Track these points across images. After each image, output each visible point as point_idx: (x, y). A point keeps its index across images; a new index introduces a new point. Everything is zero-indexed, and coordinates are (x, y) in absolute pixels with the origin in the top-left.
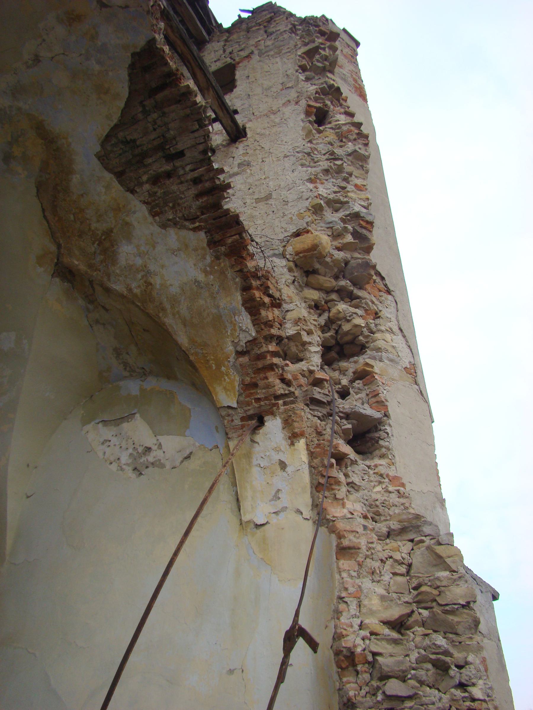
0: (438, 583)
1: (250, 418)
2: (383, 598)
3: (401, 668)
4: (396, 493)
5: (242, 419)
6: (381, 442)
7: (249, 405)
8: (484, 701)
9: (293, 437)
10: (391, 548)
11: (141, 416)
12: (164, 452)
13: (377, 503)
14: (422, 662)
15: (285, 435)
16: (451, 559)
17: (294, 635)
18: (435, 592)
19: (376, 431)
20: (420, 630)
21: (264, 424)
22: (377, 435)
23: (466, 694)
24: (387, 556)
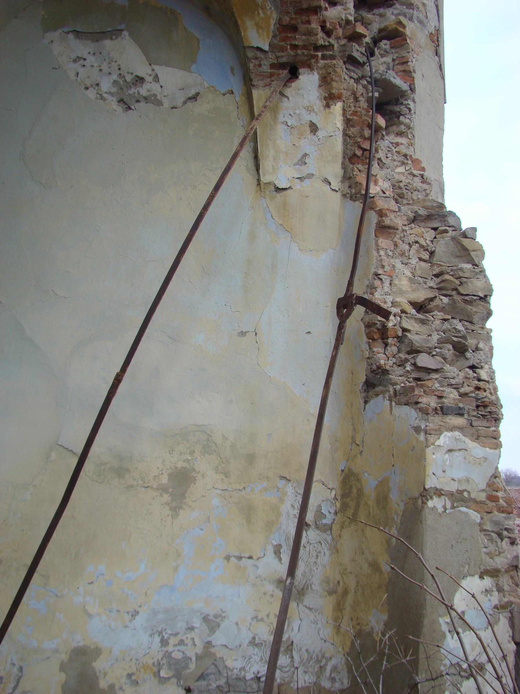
0: (461, 274)
1: (282, 66)
2: (411, 280)
3: (428, 345)
4: (420, 177)
5: (272, 66)
6: (402, 118)
7: (283, 51)
8: (488, 382)
9: (330, 99)
10: (417, 233)
11: (131, 35)
12: (161, 87)
13: (401, 185)
14: (443, 343)
15: (321, 94)
16: (475, 253)
17: (352, 303)
18: (457, 282)
19: (396, 105)
20: (440, 315)
21: (297, 78)
22: (397, 109)
23: (475, 375)
24: (413, 241)
